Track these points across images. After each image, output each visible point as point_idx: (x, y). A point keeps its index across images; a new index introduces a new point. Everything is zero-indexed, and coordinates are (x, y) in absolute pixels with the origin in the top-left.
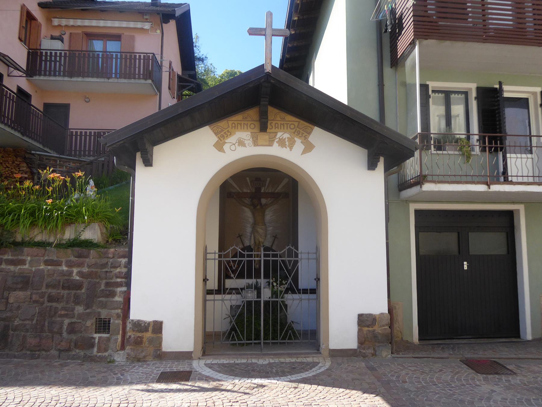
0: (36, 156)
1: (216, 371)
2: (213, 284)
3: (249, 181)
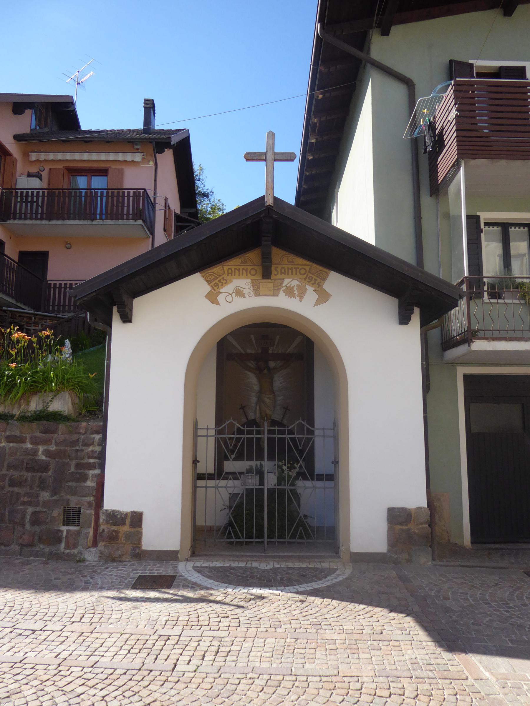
0: (8, 312)
1: (206, 576)
2: (208, 465)
3: (253, 339)
